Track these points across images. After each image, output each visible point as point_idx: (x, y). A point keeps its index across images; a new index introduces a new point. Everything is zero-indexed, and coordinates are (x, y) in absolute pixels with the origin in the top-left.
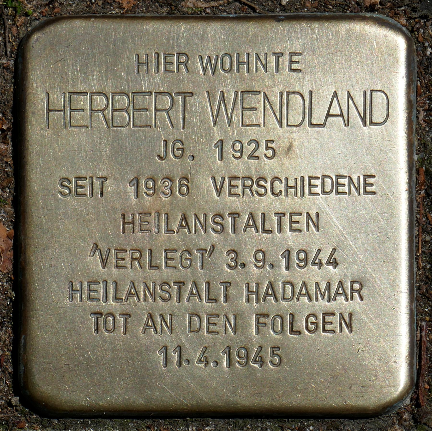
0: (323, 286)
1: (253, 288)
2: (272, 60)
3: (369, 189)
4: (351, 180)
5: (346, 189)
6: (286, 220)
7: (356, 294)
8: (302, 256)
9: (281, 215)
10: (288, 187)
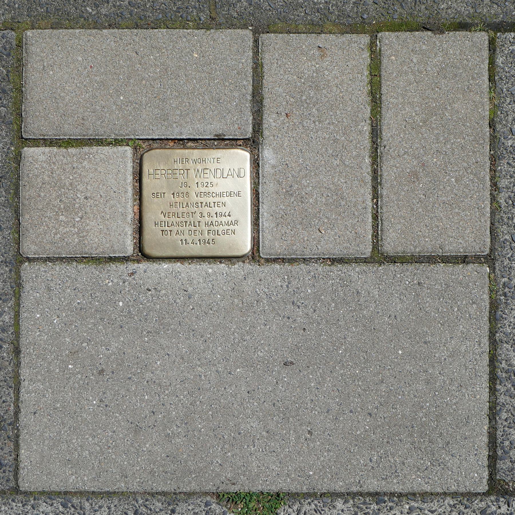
0: (226, 222)
3: (239, 195)
4: (234, 193)
5: (233, 195)
6: (216, 204)
7: (236, 224)
8: (220, 214)
10: (216, 195)
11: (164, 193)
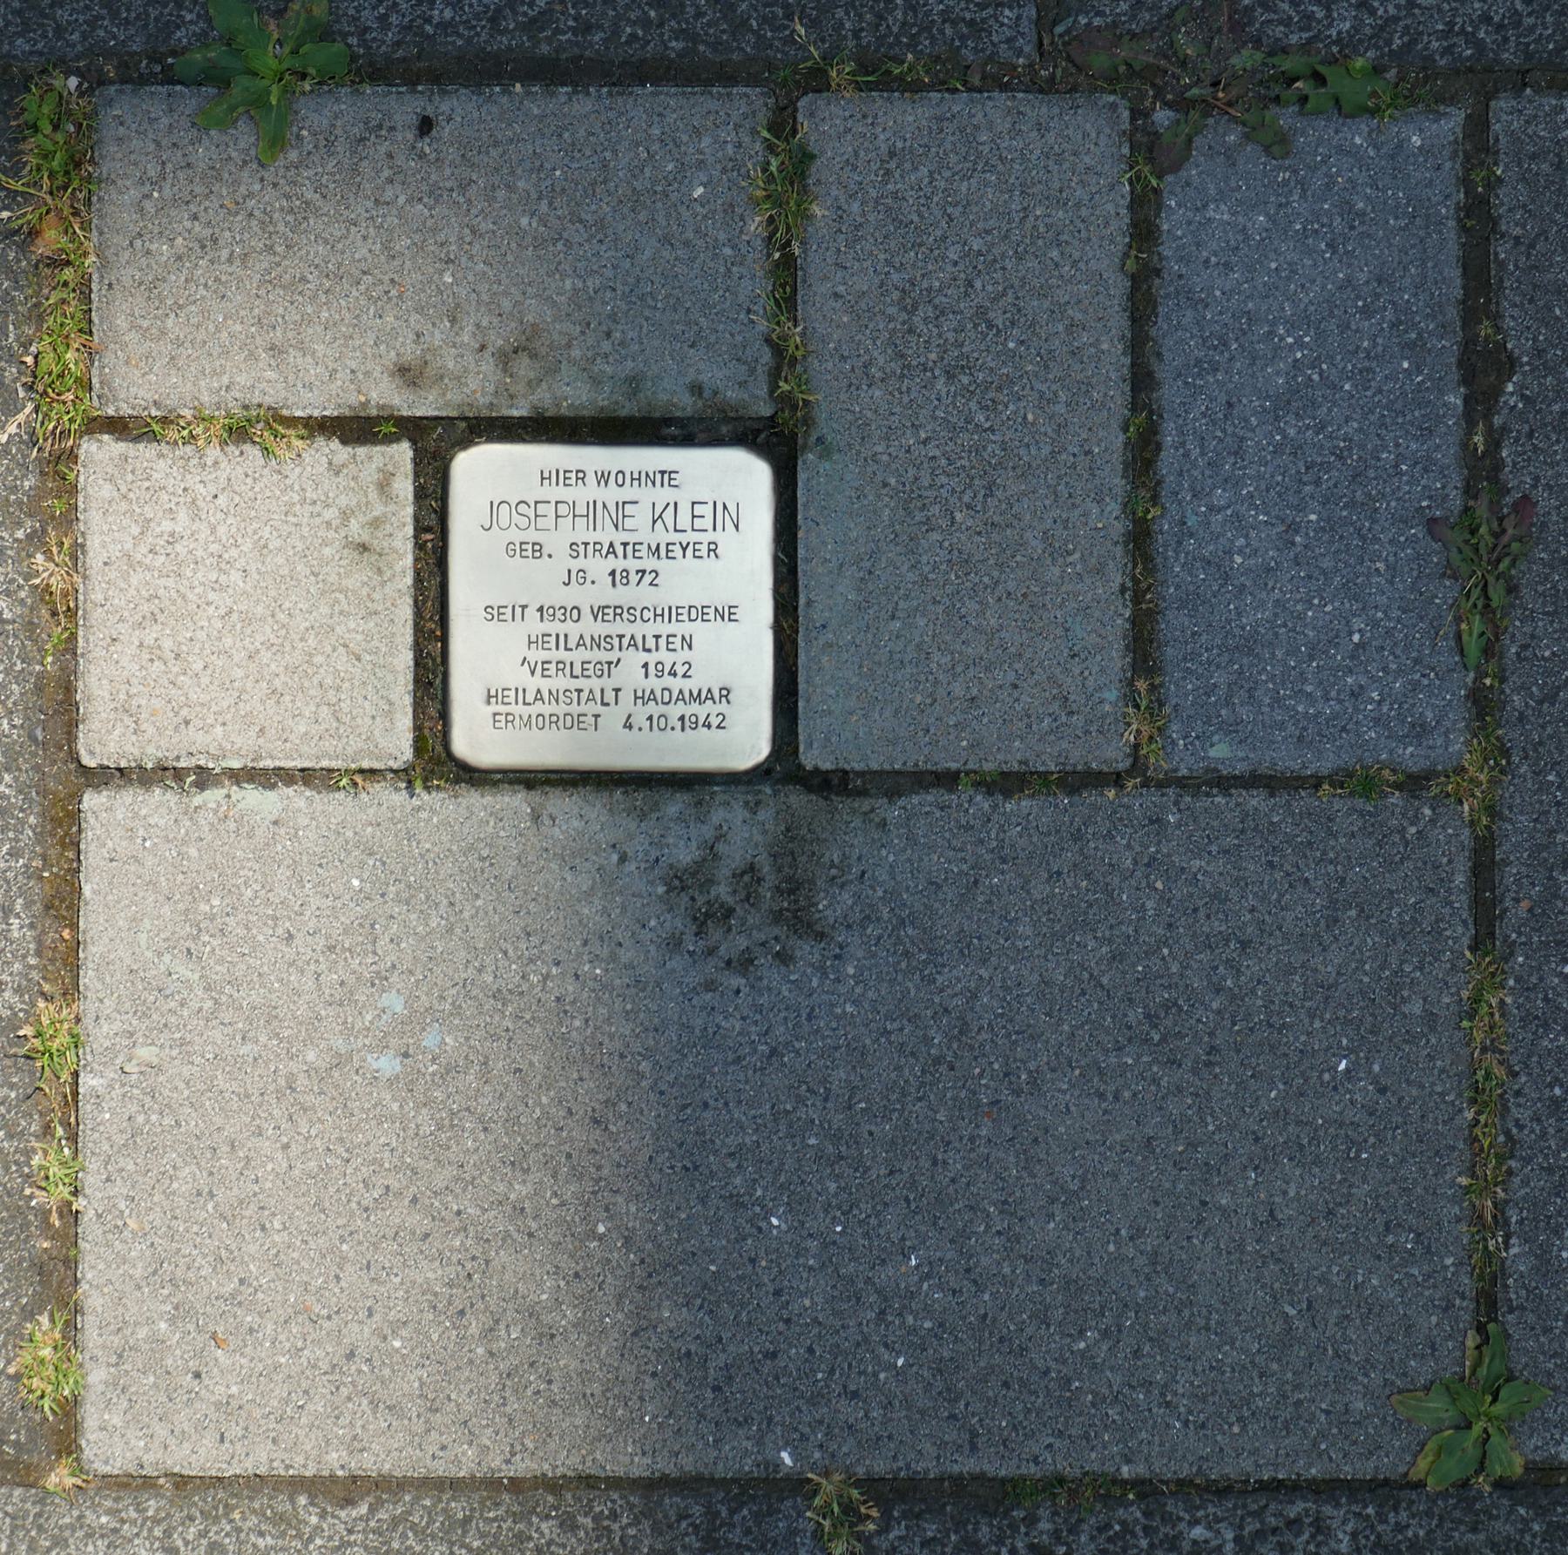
1: (640, 694)
2: (658, 476)
6: (662, 642)
9: (657, 637)
11: (524, 607)
